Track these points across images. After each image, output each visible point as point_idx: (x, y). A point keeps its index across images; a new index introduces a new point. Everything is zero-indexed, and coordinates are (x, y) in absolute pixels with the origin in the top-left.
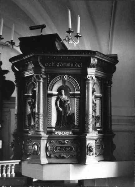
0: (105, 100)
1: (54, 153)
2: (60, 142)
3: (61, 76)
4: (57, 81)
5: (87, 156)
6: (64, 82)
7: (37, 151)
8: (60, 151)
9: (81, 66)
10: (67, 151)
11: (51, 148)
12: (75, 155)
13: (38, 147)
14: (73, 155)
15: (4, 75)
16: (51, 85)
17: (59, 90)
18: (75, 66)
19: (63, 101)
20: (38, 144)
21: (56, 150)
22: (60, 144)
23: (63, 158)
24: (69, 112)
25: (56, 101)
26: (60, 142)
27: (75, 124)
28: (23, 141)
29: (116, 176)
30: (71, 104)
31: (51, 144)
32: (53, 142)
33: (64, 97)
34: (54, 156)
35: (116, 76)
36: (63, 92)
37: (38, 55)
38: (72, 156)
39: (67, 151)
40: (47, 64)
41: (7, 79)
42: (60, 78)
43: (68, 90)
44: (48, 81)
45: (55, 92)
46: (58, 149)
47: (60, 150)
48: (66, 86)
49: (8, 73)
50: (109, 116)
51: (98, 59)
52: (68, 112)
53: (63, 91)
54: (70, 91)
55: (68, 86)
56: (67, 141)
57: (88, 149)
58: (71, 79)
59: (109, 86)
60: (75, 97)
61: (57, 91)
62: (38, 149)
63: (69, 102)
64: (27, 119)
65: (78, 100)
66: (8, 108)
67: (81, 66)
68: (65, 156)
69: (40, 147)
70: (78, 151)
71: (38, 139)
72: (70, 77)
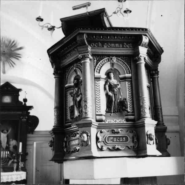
0: (153, 89)
1: (106, 145)
2: (113, 131)
3: (109, 58)
4: (104, 64)
5: (148, 146)
6: (112, 65)
7: (87, 141)
8: (114, 142)
9: (131, 47)
10: (121, 142)
11: (102, 138)
12: (131, 147)
13: (88, 136)
14: (129, 146)
15: (29, 111)
16: (104, 61)
17: (108, 74)
18: (124, 46)
19: (112, 84)
20: (88, 132)
21: (108, 140)
22: (112, 133)
23: (118, 150)
24: (120, 97)
25: (105, 85)
26: (113, 131)
27: (127, 111)
28: (65, 137)
29: (180, 174)
30: (121, 88)
31: (102, 134)
32: (104, 132)
33: (113, 81)
34: (106, 148)
35: (161, 67)
36: (112, 75)
37: (83, 32)
38: (128, 147)
39: (121, 142)
40: (93, 45)
41: (31, 114)
42: (107, 60)
43: (117, 73)
44: (95, 63)
45: (103, 75)
46: (111, 140)
47: (113, 140)
48: (115, 69)
49: (33, 109)
50: (160, 107)
51: (149, 40)
52: (119, 97)
53: (112, 73)
54: (120, 75)
55: (117, 68)
56: (121, 129)
57: (147, 137)
58: (119, 61)
59: (156, 76)
60: (126, 81)
61: (105, 75)
62: (88, 138)
63: (119, 87)
64: (69, 112)
65: (130, 83)
66: (32, 141)
67: (131, 47)
68: (119, 147)
69: (90, 136)
70: (135, 140)
71: (87, 127)
72: (119, 59)
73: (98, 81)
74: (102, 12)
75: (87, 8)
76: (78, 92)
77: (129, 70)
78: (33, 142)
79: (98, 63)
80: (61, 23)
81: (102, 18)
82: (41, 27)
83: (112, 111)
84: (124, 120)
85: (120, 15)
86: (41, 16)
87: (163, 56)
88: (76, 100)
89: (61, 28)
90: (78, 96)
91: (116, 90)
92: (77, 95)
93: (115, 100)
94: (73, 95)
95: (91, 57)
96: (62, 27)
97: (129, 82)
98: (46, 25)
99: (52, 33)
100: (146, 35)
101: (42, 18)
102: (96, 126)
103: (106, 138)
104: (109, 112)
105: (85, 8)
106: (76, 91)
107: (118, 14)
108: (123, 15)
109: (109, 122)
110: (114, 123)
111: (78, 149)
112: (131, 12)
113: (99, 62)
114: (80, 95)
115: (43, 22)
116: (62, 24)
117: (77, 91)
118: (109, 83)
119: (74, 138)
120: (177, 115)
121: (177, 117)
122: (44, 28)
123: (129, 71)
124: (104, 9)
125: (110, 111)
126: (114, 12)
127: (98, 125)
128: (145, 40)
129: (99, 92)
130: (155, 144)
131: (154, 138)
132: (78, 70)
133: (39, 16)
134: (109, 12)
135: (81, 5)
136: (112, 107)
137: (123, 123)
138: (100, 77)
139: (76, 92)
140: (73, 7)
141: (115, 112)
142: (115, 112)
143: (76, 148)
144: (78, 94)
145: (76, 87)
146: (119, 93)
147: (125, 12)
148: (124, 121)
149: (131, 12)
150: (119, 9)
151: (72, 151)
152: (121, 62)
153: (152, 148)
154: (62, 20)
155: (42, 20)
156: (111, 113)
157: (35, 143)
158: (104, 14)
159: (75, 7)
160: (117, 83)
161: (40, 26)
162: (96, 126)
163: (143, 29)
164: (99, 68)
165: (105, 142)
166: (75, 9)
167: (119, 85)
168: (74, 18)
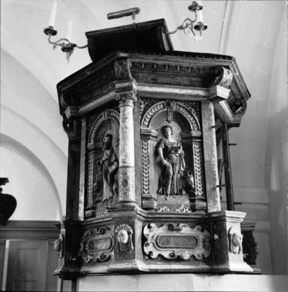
3: (165, 102)
13: (129, 233)
16: (156, 108)
41: (4, 192)
66: (3, 238)
73: (145, 141)
74: (160, 24)
75: (134, 18)
76: (110, 157)
77: (197, 123)
78: (4, 239)
79: (147, 109)
80: (86, 39)
81: (159, 34)
82: (52, 45)
83: (169, 193)
84: (188, 208)
85: (188, 32)
86: (53, 26)
87: (249, 102)
88: (108, 170)
89: (87, 48)
90: (111, 164)
91: (174, 157)
92: (110, 162)
93: (174, 174)
94: (101, 162)
95: (136, 99)
96: (88, 46)
97: (197, 144)
98: (61, 42)
99: (69, 55)
100: (228, 67)
101: (55, 29)
102: (142, 216)
103: (157, 238)
104: (163, 194)
105: (130, 17)
106: (107, 155)
107: (185, 29)
108: (193, 32)
109: (162, 211)
110: (172, 212)
111: (107, 257)
112: (206, 27)
113: (149, 108)
114: (115, 163)
115: (57, 34)
116: (88, 41)
117: (109, 156)
118: (165, 145)
119: (101, 236)
120: (267, 202)
121: (265, 207)
122: (57, 46)
123: (198, 126)
124: (163, 20)
125: (165, 193)
126: (180, 25)
127: (145, 216)
128: (227, 76)
129: (147, 159)
130: (241, 252)
131: (241, 241)
132: (113, 120)
133: (51, 27)
134: (171, 26)
135: (118, 12)
136: (168, 185)
137: (187, 213)
138: (149, 134)
139: (107, 157)
140: (108, 14)
141: (174, 194)
142: (174, 194)
143: (105, 254)
144: (112, 160)
145: (108, 149)
146: (180, 164)
147: (197, 28)
148: (189, 209)
149: (206, 27)
150: (189, 22)
151: (98, 259)
152: (184, 110)
153: (236, 261)
154: (88, 35)
155: (54, 33)
156: (167, 195)
157: (8, 242)
158: (163, 28)
159: (112, 13)
160: (177, 144)
161: (50, 42)
162: (142, 216)
163: (224, 57)
164: (148, 118)
165: (156, 245)
166: (111, 17)
167: (180, 149)
168: (110, 32)
